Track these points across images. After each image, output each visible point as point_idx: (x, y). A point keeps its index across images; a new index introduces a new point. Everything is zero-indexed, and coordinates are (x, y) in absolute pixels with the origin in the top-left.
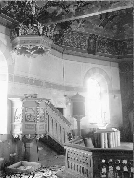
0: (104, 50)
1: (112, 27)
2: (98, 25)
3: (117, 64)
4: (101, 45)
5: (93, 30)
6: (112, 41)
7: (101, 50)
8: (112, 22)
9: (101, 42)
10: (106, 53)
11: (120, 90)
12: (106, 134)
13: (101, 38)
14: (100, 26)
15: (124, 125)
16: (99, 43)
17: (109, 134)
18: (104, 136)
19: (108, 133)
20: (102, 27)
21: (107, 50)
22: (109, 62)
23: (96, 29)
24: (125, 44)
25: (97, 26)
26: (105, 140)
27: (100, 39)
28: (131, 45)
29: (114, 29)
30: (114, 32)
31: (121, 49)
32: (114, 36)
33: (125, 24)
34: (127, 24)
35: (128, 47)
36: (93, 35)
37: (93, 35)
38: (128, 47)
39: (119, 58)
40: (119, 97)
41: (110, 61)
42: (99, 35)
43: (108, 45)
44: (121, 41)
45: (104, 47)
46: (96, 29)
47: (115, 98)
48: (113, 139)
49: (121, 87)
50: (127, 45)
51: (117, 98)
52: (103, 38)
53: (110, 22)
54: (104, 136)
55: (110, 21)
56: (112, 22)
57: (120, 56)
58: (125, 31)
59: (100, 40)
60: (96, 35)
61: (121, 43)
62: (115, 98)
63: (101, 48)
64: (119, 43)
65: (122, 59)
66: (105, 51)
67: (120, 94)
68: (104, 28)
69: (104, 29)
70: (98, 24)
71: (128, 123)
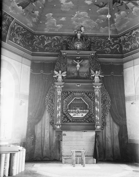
0: (17, 39)
1: (34, 13)
2: (18, 4)
3: (29, 62)
4: (15, 33)
5: (10, 8)
6: (29, 31)
7: (13, 39)
8: (35, 5)
9: (16, 29)
10: (19, 44)
11: (28, 95)
12: (9, 155)
13: (17, 23)
14: (19, 5)
15: (27, 140)
16: (13, 29)
17: (12, 155)
18: (6, 158)
19: (11, 154)
20: (22, 8)
21: (20, 41)
22: (21, 57)
23: (13, 8)
24: (43, 40)
25: (16, 4)
26: (5, 165)
27: (15, 24)
28: (50, 42)
29: (35, 16)
30: (34, 20)
31: (37, 45)
32: (32, 26)
33: (50, 13)
34: (51, 14)
35: (46, 43)
36: (7, 15)
37: (7, 15)
38: (46, 43)
39: (33, 55)
40: (26, 104)
41: (22, 56)
42: (15, 18)
43: (23, 35)
44: (39, 35)
45: (18, 36)
46: (13, 8)
47: (21, 104)
48: (17, 162)
49: (30, 91)
50: (45, 41)
51: (24, 104)
52: (19, 25)
53: (32, 4)
54: (6, 158)
55: (33, 4)
56: (35, 5)
57: (35, 54)
58: (46, 22)
59: (15, 26)
60: (12, 18)
61: (39, 37)
62: (21, 104)
63: (13, 36)
64: (36, 36)
65: (103, 8)
66: (19, 42)
67: (28, 100)
68: (23, 10)
69: (22, 11)
70: (18, 2)
71: (33, 137)
